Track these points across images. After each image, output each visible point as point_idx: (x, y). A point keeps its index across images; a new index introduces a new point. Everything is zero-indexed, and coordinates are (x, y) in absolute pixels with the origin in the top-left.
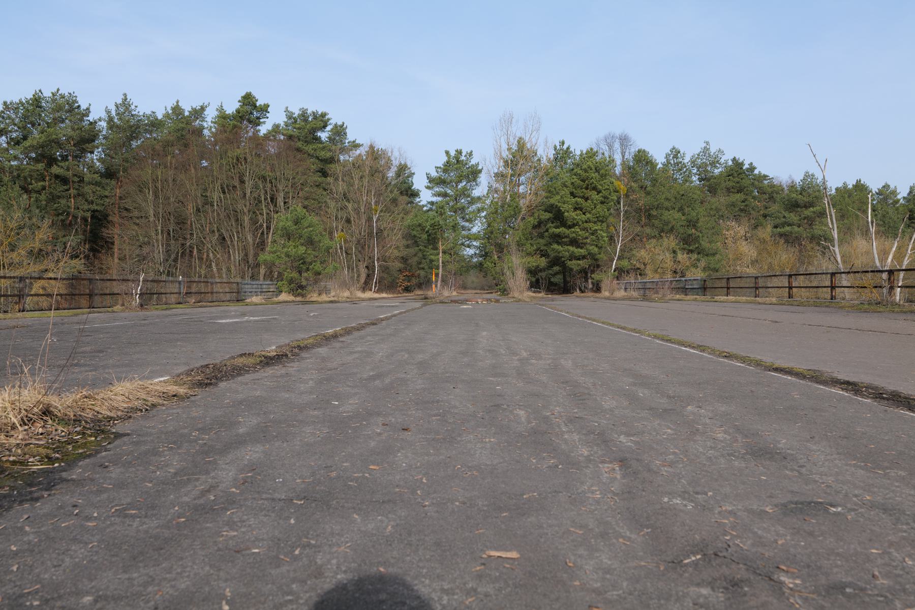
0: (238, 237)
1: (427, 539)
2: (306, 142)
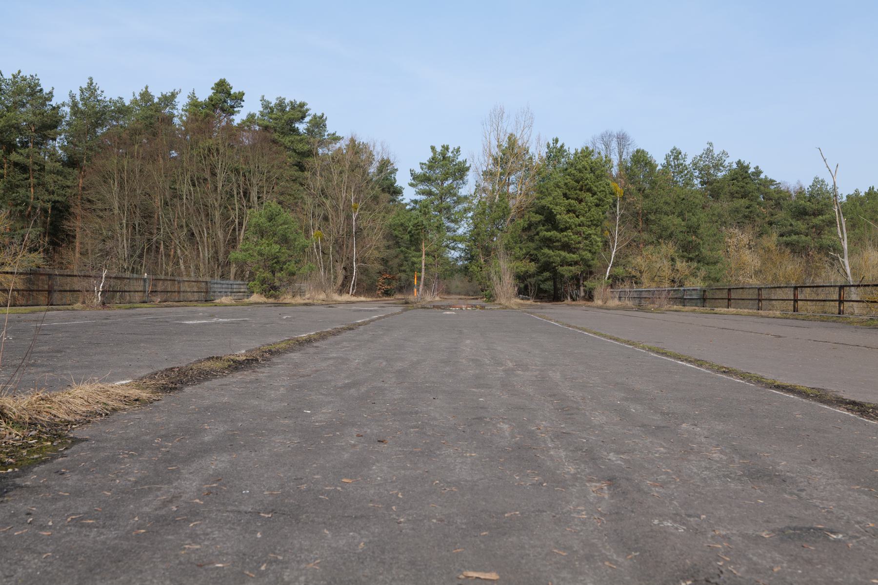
0: (208, 233)
1: (401, 557)
2: (282, 133)
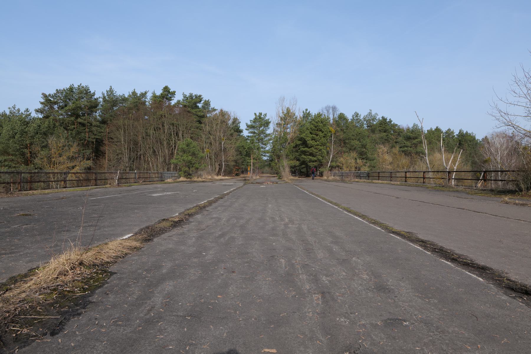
0: (161, 151)
1: (240, 340)
2: (192, 108)
